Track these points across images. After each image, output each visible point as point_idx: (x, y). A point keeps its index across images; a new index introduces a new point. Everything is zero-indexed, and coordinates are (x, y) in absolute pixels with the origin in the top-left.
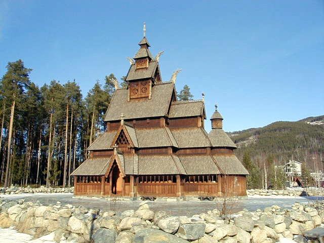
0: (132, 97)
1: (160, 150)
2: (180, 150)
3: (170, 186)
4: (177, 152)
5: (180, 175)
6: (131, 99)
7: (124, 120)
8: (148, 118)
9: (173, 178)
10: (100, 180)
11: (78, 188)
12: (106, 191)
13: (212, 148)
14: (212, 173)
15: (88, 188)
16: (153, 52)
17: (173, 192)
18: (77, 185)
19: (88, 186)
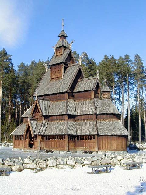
0: (52, 77)
1: (59, 117)
2: (78, 116)
3: (62, 143)
4: (76, 118)
5: (68, 135)
6: (52, 79)
7: (38, 96)
8: (43, 95)
9: (62, 137)
10: (94, 138)
11: (15, 143)
12: (26, 145)
13: (97, 115)
14: (91, 134)
15: (20, 143)
16: (68, 42)
17: (64, 147)
18: (15, 141)
19: (20, 142)
